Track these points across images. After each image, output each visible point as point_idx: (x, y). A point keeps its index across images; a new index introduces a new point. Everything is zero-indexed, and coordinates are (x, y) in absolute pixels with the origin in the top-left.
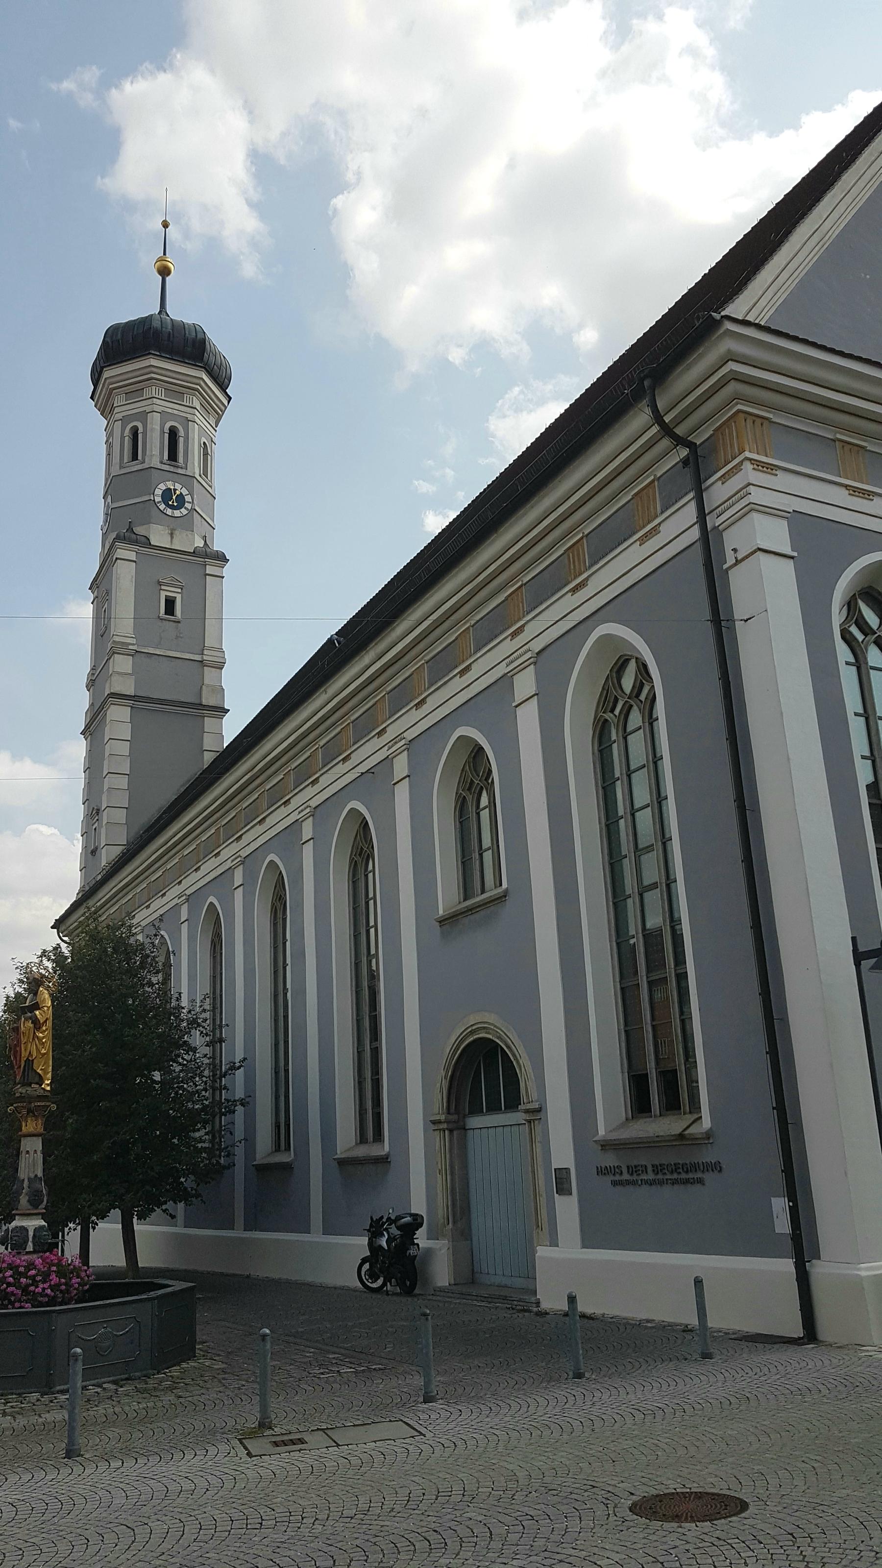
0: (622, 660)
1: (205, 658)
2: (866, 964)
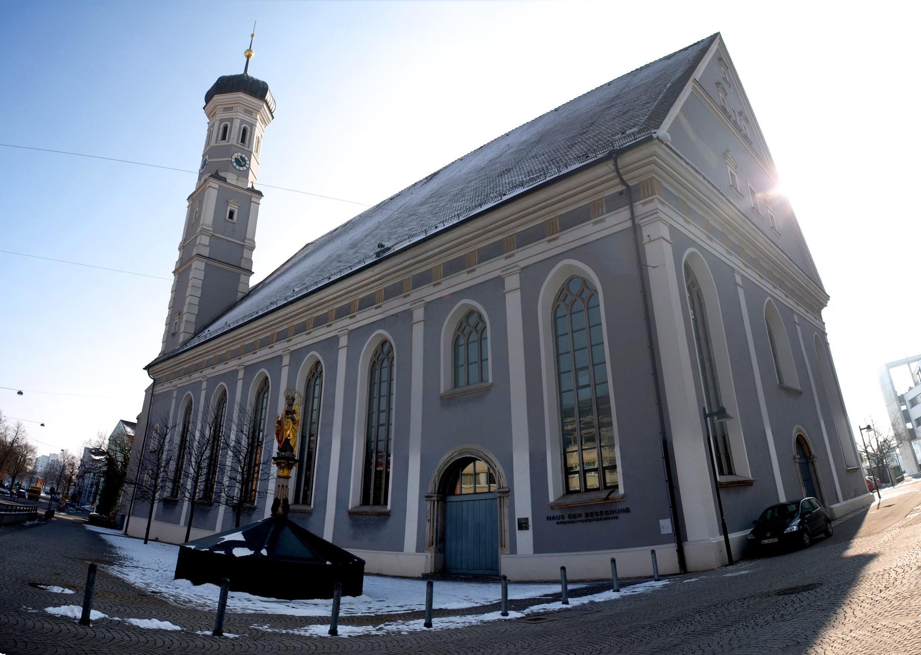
0: (572, 277)
1: (245, 244)
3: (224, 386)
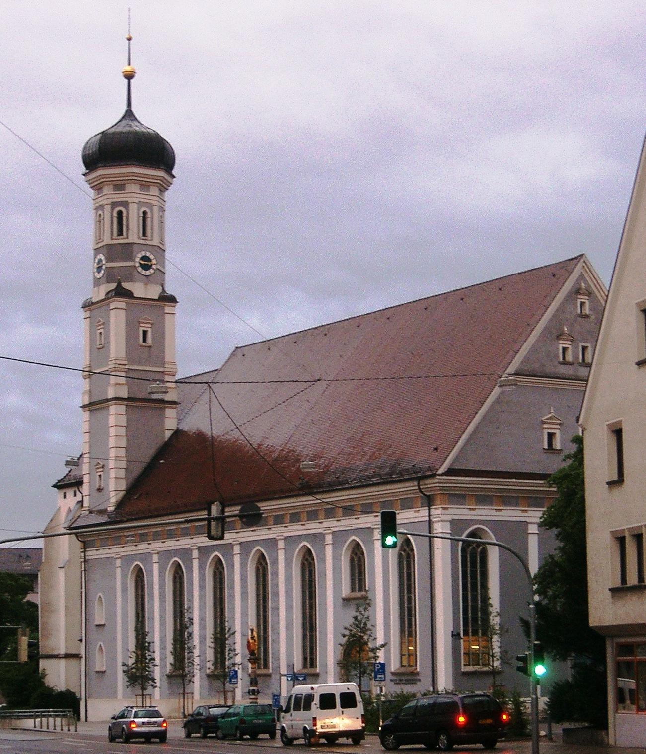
3: (307, 546)
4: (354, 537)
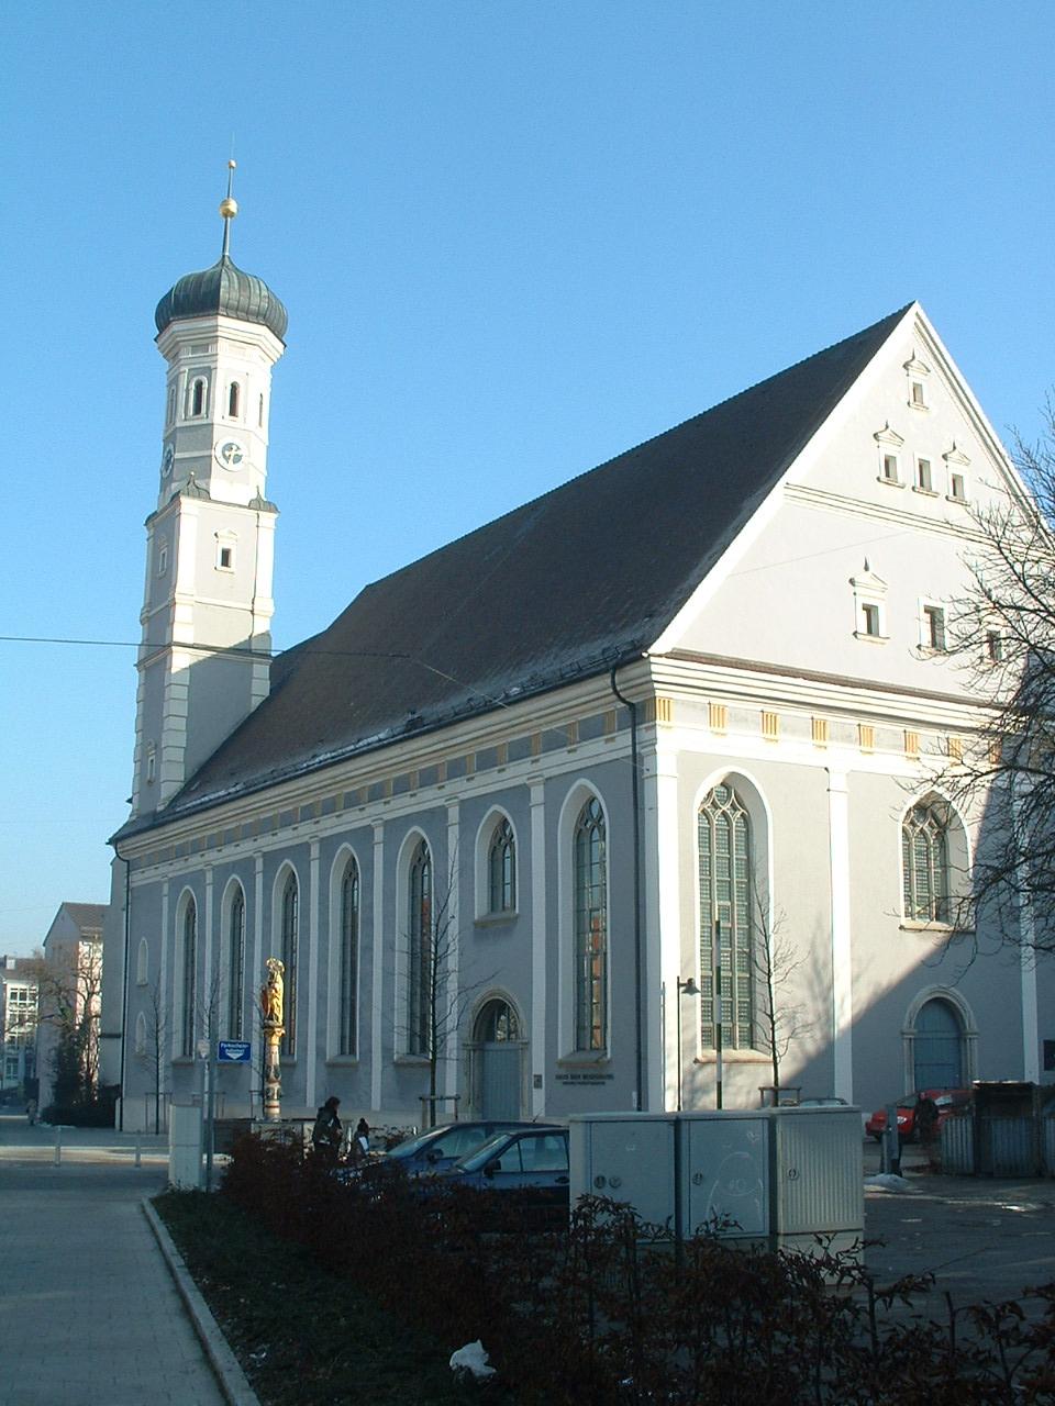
2: (682, 989)
3: (419, 834)
4: (496, 807)
